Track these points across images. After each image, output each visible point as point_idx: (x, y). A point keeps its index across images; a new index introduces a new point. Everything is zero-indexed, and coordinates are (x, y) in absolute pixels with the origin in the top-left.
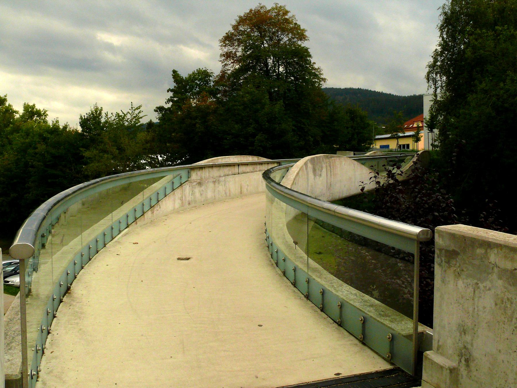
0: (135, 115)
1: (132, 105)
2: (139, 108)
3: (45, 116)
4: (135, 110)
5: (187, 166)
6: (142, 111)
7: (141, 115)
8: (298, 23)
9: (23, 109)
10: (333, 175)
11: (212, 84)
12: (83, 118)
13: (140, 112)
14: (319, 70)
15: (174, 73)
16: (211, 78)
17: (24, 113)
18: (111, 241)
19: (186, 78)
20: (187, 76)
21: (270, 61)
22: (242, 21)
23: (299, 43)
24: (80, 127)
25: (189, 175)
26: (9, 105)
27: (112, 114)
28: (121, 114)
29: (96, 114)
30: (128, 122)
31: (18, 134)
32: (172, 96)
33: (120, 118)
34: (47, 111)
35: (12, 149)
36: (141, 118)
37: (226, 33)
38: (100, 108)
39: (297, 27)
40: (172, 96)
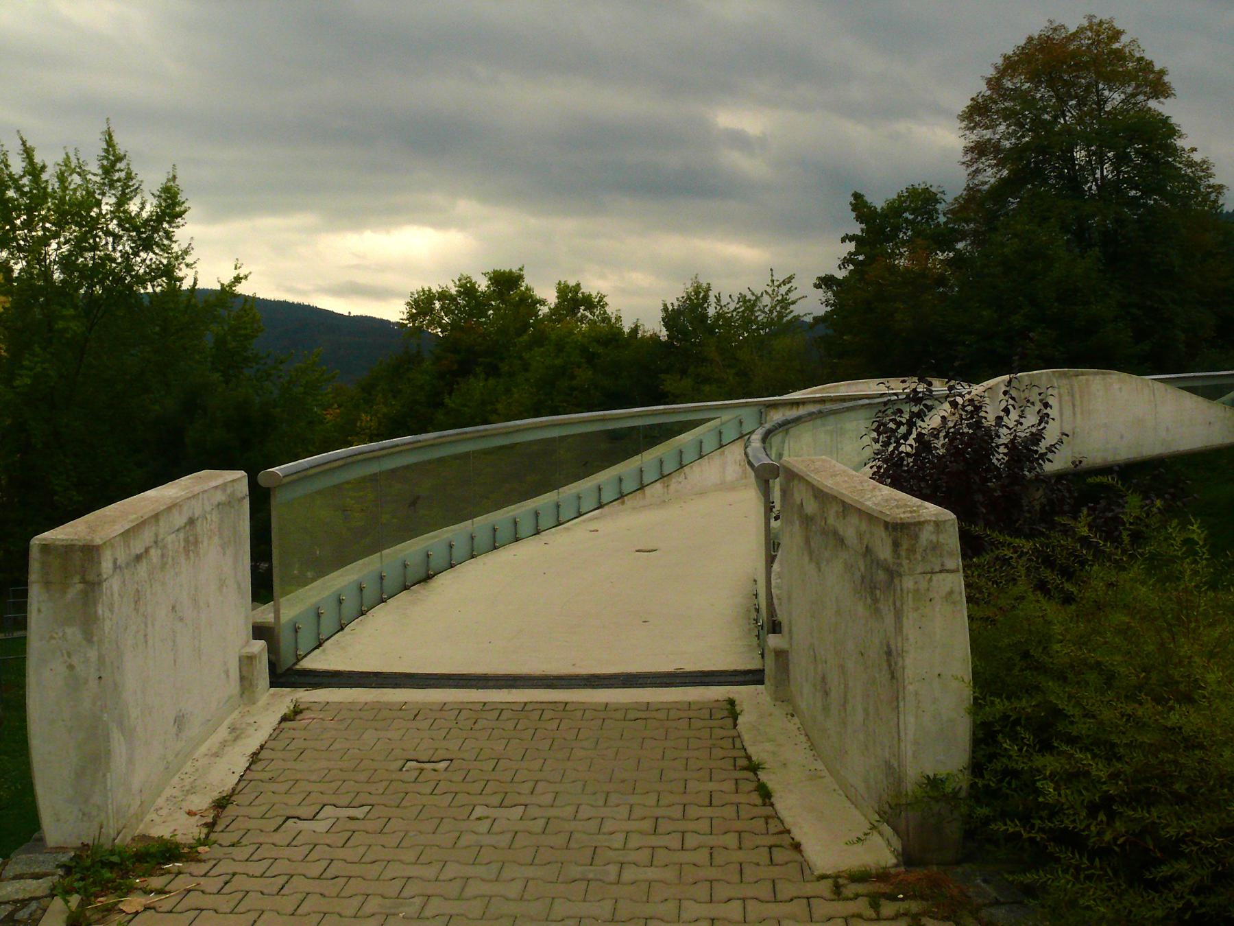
0: (780, 298)
1: (772, 275)
2: (790, 279)
3: (603, 306)
4: (779, 286)
5: (756, 400)
6: (796, 288)
7: (792, 297)
8: (1148, 56)
9: (556, 294)
10: (1082, 413)
11: (942, 219)
12: (670, 308)
13: (789, 290)
14: (1205, 166)
15: (855, 199)
16: (938, 206)
17: (559, 303)
18: (553, 527)
19: (882, 208)
20: (884, 205)
21: (1080, 155)
22: (1010, 66)
23: (1152, 104)
24: (664, 329)
25: (763, 419)
26: (527, 288)
27: (730, 296)
28: (749, 296)
29: (697, 298)
30: (764, 312)
31: (542, 349)
32: (853, 250)
33: (749, 304)
34: (604, 296)
35: (527, 380)
36: (794, 303)
37: (972, 99)
38: (705, 285)
39: (1145, 66)
40: (853, 250)
